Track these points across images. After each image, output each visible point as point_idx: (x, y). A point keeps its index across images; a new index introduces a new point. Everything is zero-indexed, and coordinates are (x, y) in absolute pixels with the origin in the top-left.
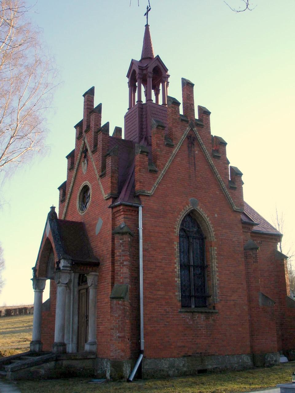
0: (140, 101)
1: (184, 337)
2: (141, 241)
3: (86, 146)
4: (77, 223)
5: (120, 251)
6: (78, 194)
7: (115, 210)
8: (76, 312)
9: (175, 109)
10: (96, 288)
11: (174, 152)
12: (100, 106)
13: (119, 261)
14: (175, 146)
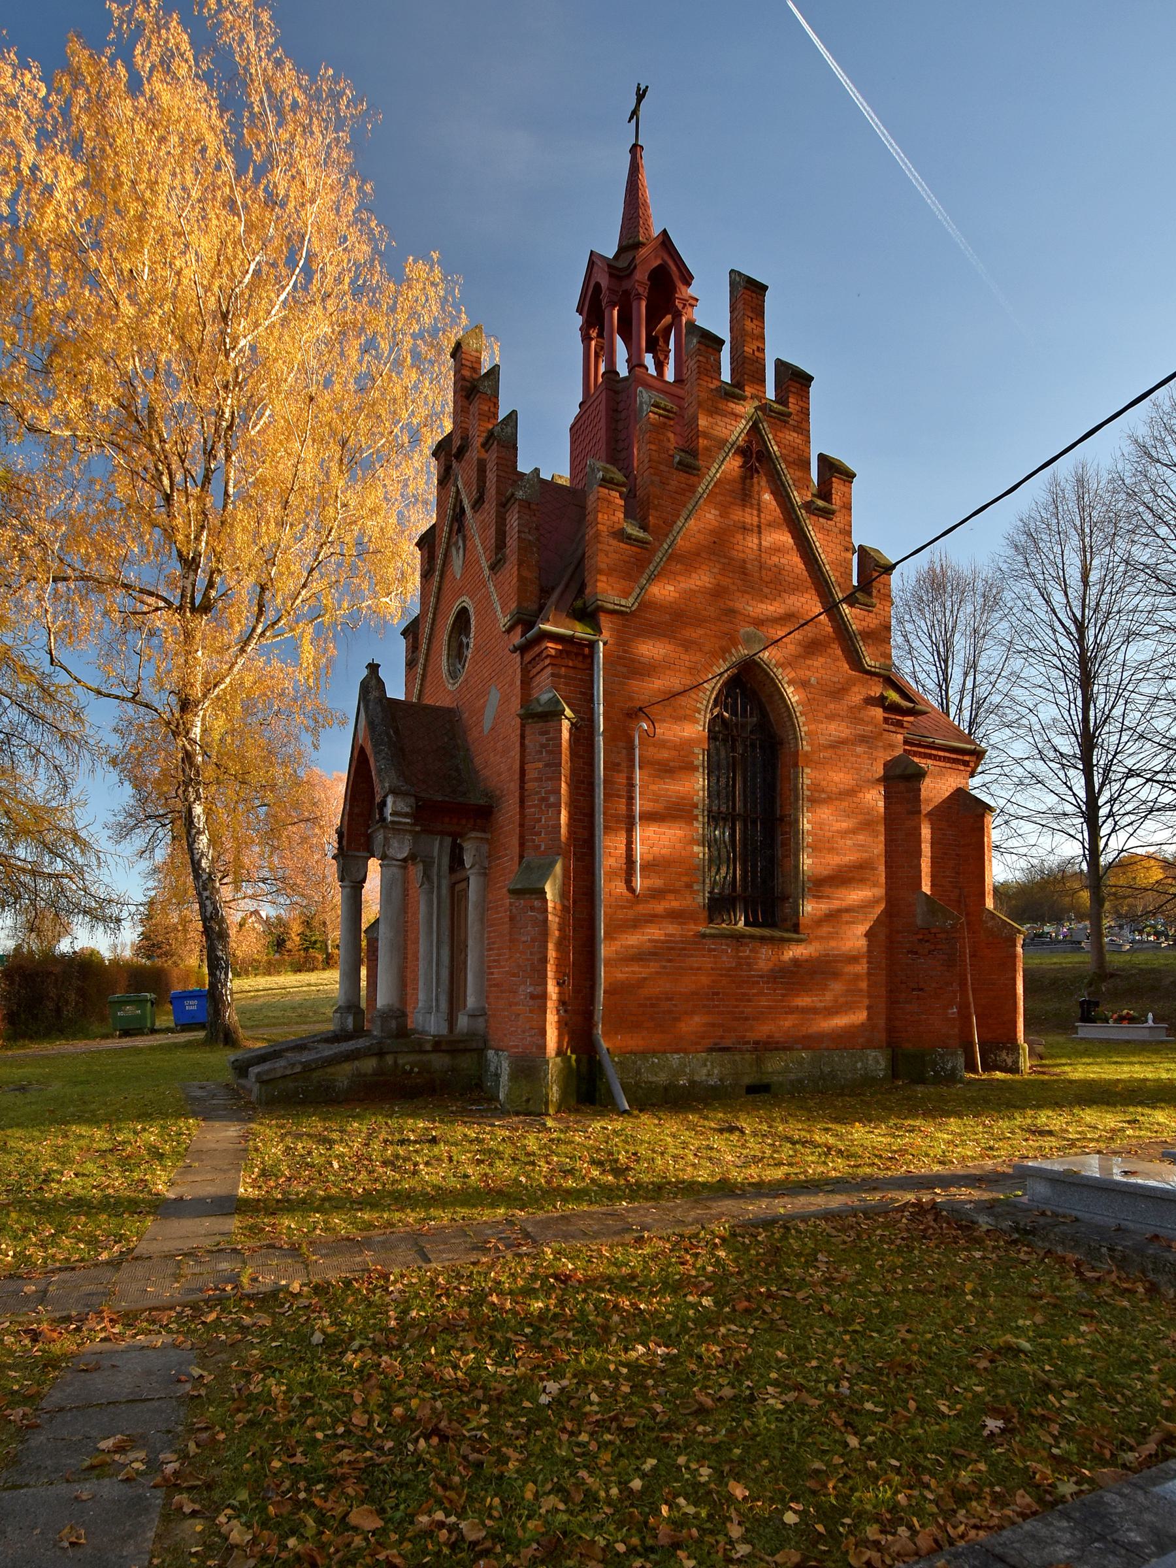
0: (611, 372)
1: (713, 1000)
2: (600, 742)
3: (461, 501)
4: (439, 709)
5: (540, 765)
6: (446, 638)
7: (528, 657)
8: (446, 938)
9: (707, 358)
10: (485, 874)
11: (700, 490)
12: (513, 416)
13: (538, 793)
14: (704, 470)
